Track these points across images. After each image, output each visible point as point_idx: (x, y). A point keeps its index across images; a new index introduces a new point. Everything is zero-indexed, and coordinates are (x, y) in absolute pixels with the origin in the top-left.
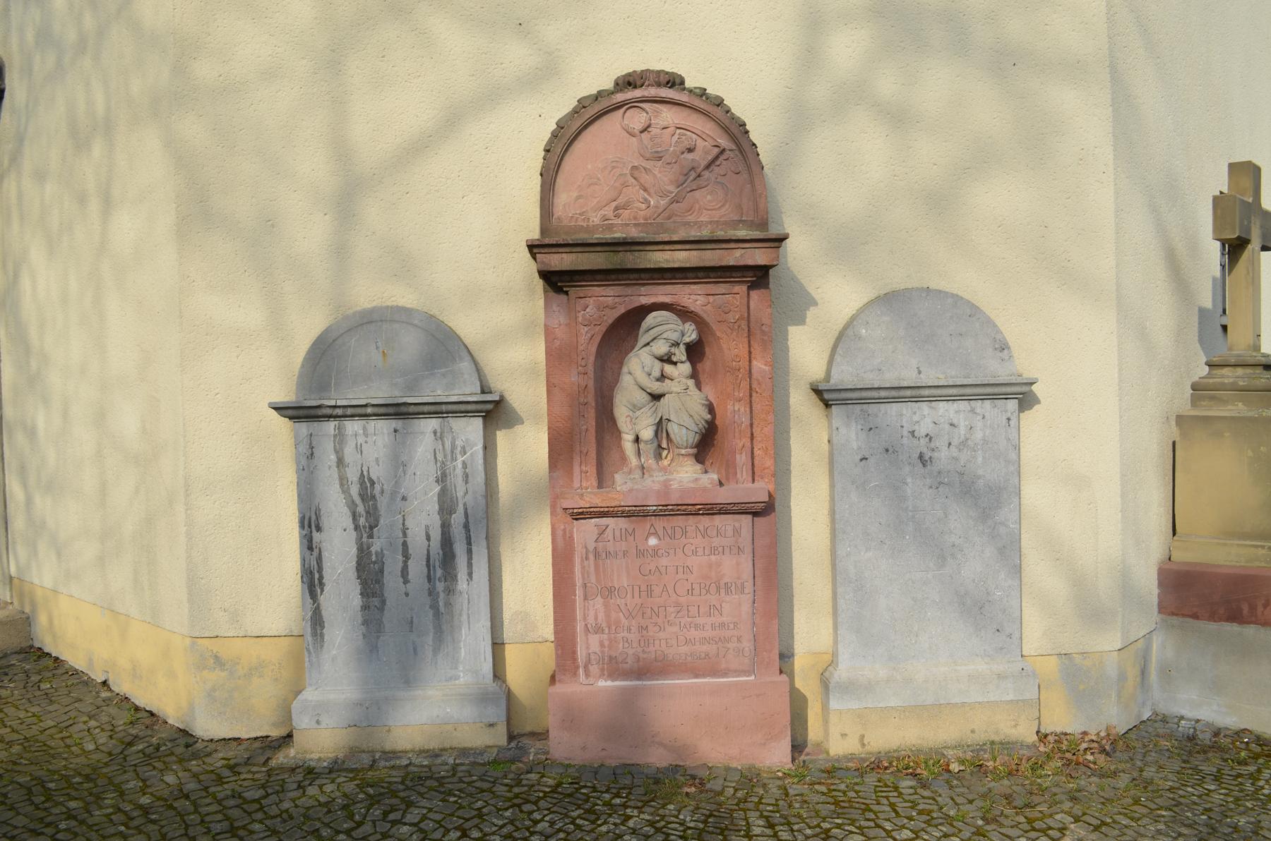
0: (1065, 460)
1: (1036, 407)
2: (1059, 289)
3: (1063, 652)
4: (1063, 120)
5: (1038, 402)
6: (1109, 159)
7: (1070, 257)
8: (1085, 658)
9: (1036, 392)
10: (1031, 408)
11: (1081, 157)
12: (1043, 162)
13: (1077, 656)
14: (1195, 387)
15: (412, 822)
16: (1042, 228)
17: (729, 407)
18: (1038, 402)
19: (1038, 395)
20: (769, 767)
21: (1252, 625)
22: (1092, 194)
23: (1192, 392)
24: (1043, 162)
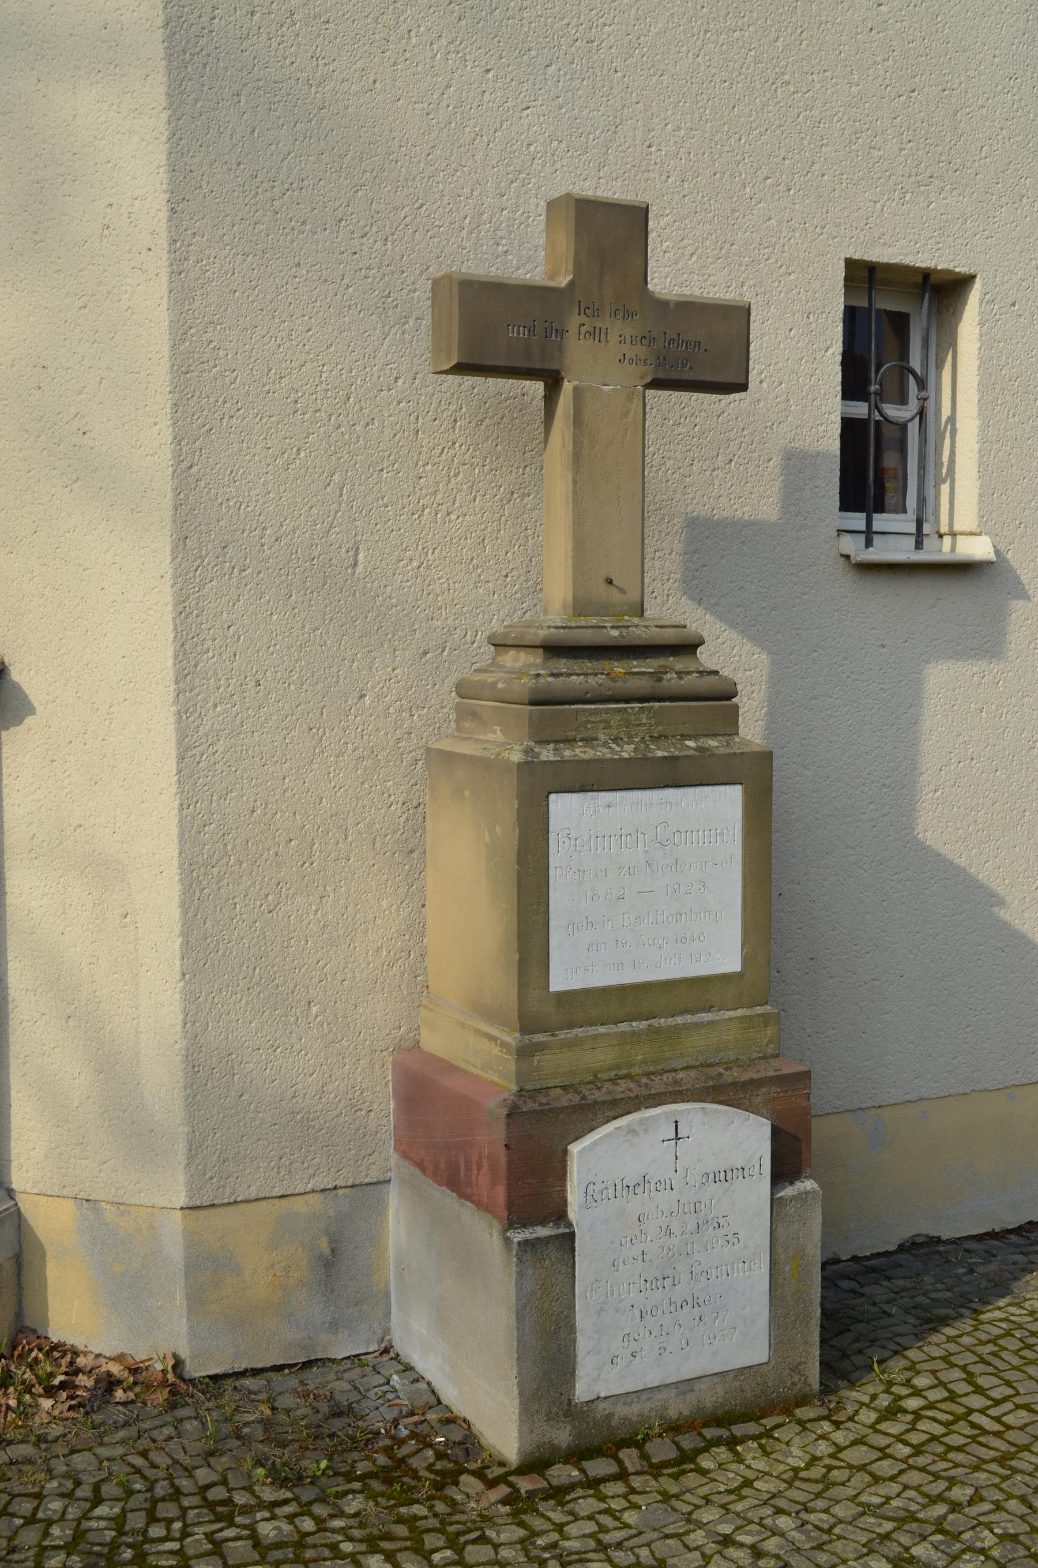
0: (80, 826)
1: (29, 721)
2: (68, 489)
3: (82, 1195)
4: (75, 150)
5: (32, 711)
6: (159, 221)
7: (86, 424)
8: (122, 1214)
9: (27, 692)
10: (20, 722)
11: (106, 221)
12: (38, 238)
13: (108, 1207)
14: (463, 690)
15: (982, 1456)
16: (36, 369)
17: (625, 755)
18: (32, 711)
19: (30, 697)
20: (72, 1346)
21: (469, 1204)
22: (127, 296)
23: (459, 699)
24: (38, 238)
